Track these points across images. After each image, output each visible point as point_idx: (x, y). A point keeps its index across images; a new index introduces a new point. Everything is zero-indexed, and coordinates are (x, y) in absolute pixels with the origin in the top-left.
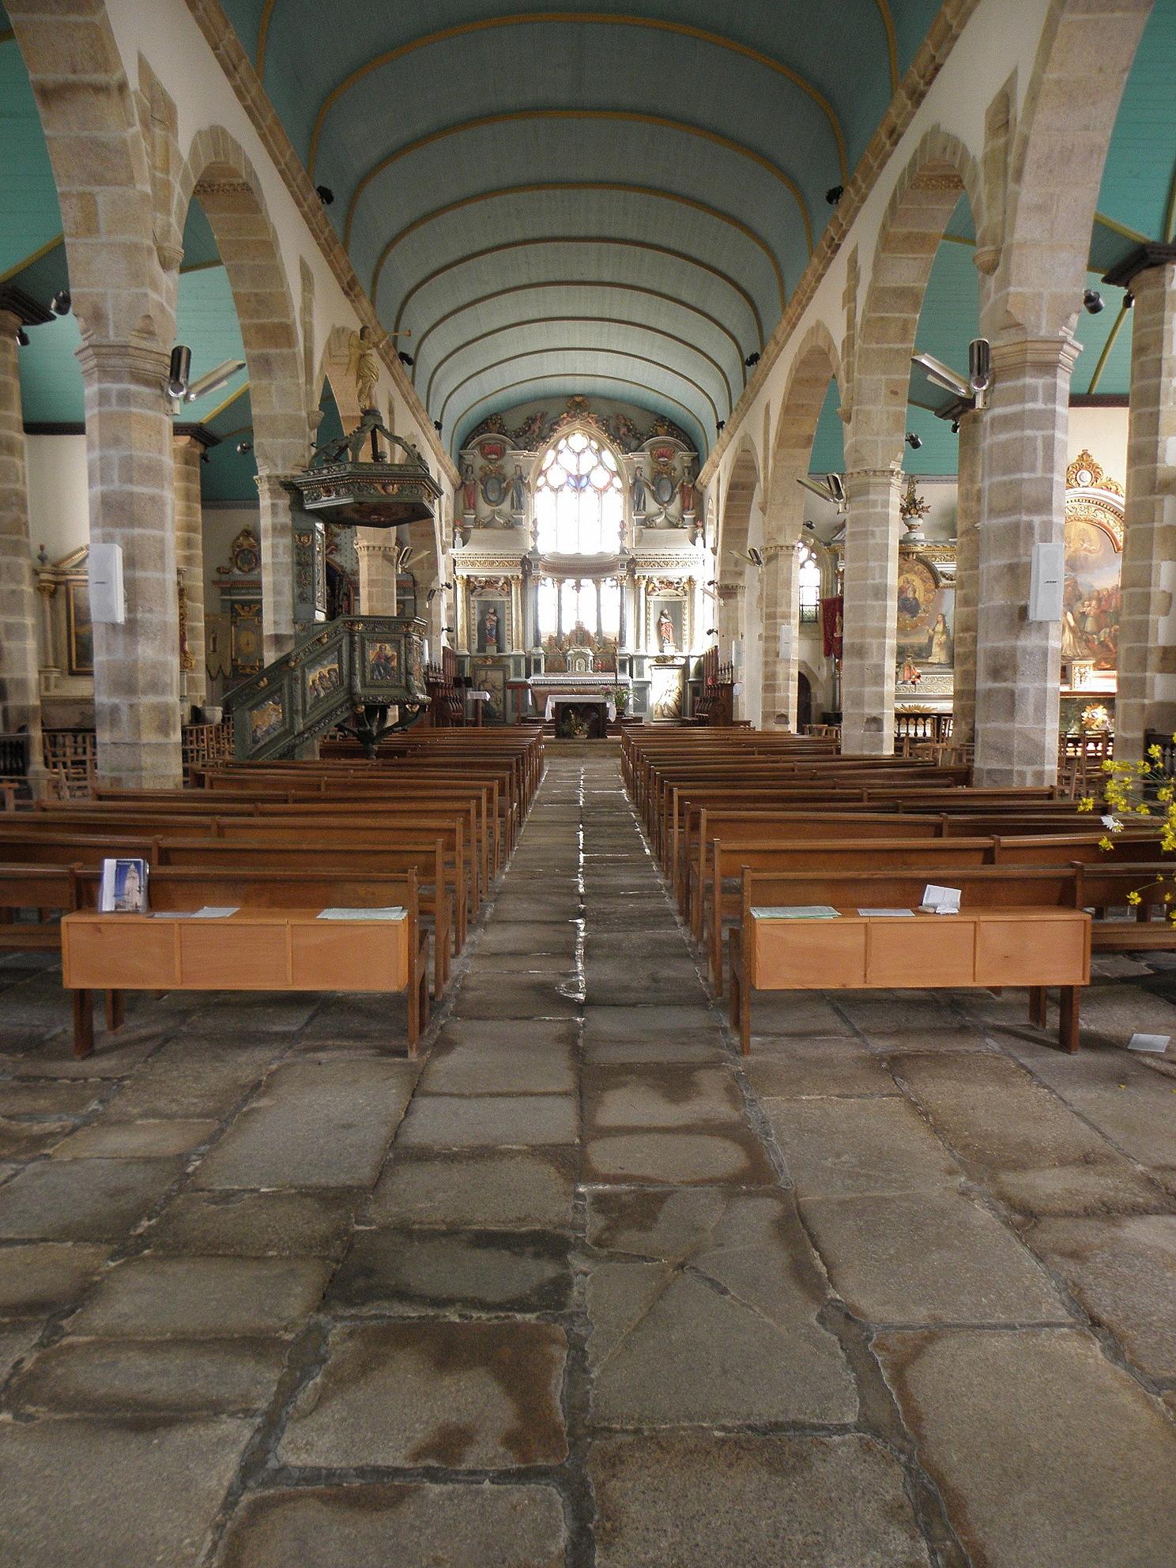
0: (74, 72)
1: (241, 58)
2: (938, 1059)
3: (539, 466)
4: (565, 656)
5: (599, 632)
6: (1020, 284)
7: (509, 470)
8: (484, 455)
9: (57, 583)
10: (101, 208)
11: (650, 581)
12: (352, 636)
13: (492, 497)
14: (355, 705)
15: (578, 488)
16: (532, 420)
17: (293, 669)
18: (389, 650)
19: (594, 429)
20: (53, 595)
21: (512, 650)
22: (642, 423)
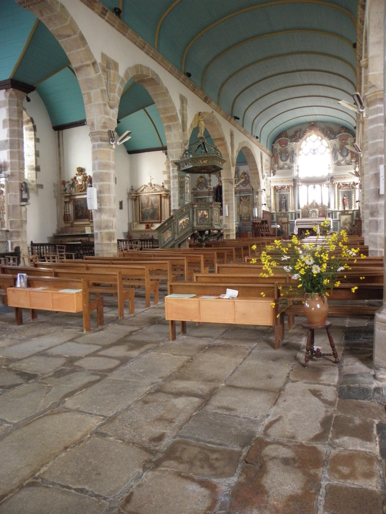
0: (82, 63)
1: (145, 44)
2: (225, 347)
3: (300, 147)
4: (308, 212)
5: (322, 203)
6: (373, 71)
7: (289, 149)
8: (281, 145)
9: (136, 197)
10: (92, 96)
11: (339, 184)
12: (193, 209)
13: (283, 159)
14: (194, 231)
15: (314, 153)
16: (296, 132)
17: (174, 220)
18: (205, 213)
19: (319, 133)
20: (135, 200)
21: (290, 210)
22: (336, 129)
